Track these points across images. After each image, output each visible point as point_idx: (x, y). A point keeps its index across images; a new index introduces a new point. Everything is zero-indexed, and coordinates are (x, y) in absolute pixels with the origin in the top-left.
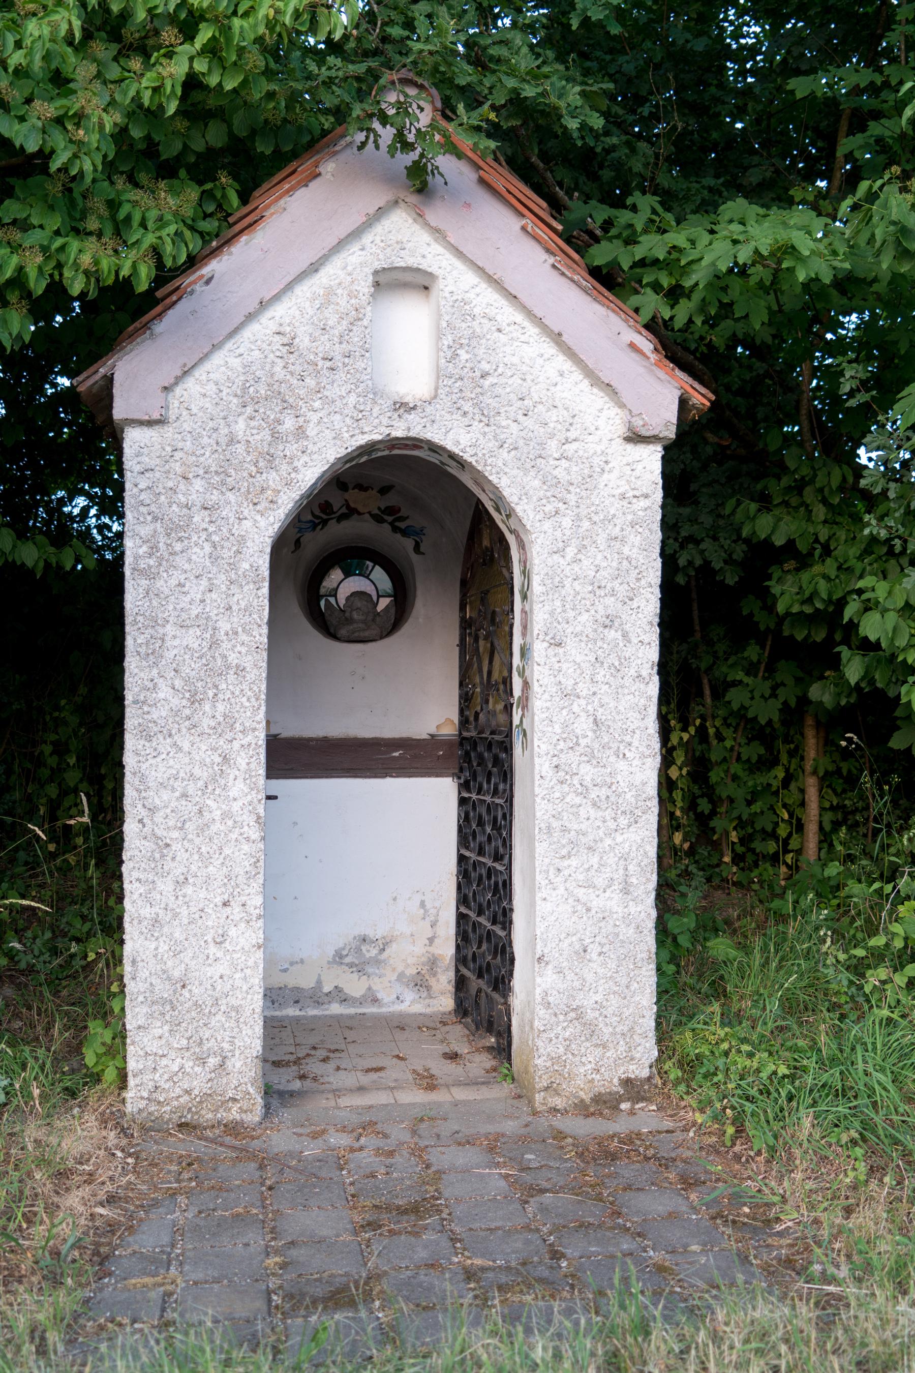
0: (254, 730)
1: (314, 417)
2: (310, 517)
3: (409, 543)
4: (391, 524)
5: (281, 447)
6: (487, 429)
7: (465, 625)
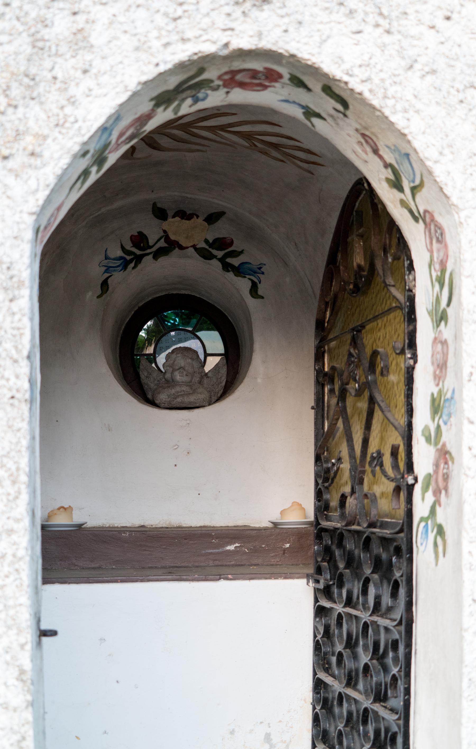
0: (10, 532)
1: (102, 14)
2: (119, 253)
3: (244, 285)
4: (222, 260)
5: (48, 64)
6: (387, 39)
7: (323, 379)
